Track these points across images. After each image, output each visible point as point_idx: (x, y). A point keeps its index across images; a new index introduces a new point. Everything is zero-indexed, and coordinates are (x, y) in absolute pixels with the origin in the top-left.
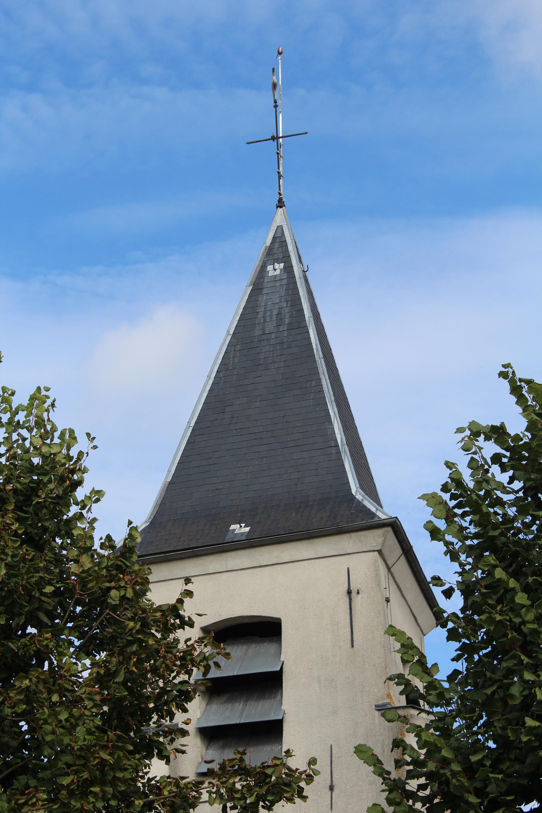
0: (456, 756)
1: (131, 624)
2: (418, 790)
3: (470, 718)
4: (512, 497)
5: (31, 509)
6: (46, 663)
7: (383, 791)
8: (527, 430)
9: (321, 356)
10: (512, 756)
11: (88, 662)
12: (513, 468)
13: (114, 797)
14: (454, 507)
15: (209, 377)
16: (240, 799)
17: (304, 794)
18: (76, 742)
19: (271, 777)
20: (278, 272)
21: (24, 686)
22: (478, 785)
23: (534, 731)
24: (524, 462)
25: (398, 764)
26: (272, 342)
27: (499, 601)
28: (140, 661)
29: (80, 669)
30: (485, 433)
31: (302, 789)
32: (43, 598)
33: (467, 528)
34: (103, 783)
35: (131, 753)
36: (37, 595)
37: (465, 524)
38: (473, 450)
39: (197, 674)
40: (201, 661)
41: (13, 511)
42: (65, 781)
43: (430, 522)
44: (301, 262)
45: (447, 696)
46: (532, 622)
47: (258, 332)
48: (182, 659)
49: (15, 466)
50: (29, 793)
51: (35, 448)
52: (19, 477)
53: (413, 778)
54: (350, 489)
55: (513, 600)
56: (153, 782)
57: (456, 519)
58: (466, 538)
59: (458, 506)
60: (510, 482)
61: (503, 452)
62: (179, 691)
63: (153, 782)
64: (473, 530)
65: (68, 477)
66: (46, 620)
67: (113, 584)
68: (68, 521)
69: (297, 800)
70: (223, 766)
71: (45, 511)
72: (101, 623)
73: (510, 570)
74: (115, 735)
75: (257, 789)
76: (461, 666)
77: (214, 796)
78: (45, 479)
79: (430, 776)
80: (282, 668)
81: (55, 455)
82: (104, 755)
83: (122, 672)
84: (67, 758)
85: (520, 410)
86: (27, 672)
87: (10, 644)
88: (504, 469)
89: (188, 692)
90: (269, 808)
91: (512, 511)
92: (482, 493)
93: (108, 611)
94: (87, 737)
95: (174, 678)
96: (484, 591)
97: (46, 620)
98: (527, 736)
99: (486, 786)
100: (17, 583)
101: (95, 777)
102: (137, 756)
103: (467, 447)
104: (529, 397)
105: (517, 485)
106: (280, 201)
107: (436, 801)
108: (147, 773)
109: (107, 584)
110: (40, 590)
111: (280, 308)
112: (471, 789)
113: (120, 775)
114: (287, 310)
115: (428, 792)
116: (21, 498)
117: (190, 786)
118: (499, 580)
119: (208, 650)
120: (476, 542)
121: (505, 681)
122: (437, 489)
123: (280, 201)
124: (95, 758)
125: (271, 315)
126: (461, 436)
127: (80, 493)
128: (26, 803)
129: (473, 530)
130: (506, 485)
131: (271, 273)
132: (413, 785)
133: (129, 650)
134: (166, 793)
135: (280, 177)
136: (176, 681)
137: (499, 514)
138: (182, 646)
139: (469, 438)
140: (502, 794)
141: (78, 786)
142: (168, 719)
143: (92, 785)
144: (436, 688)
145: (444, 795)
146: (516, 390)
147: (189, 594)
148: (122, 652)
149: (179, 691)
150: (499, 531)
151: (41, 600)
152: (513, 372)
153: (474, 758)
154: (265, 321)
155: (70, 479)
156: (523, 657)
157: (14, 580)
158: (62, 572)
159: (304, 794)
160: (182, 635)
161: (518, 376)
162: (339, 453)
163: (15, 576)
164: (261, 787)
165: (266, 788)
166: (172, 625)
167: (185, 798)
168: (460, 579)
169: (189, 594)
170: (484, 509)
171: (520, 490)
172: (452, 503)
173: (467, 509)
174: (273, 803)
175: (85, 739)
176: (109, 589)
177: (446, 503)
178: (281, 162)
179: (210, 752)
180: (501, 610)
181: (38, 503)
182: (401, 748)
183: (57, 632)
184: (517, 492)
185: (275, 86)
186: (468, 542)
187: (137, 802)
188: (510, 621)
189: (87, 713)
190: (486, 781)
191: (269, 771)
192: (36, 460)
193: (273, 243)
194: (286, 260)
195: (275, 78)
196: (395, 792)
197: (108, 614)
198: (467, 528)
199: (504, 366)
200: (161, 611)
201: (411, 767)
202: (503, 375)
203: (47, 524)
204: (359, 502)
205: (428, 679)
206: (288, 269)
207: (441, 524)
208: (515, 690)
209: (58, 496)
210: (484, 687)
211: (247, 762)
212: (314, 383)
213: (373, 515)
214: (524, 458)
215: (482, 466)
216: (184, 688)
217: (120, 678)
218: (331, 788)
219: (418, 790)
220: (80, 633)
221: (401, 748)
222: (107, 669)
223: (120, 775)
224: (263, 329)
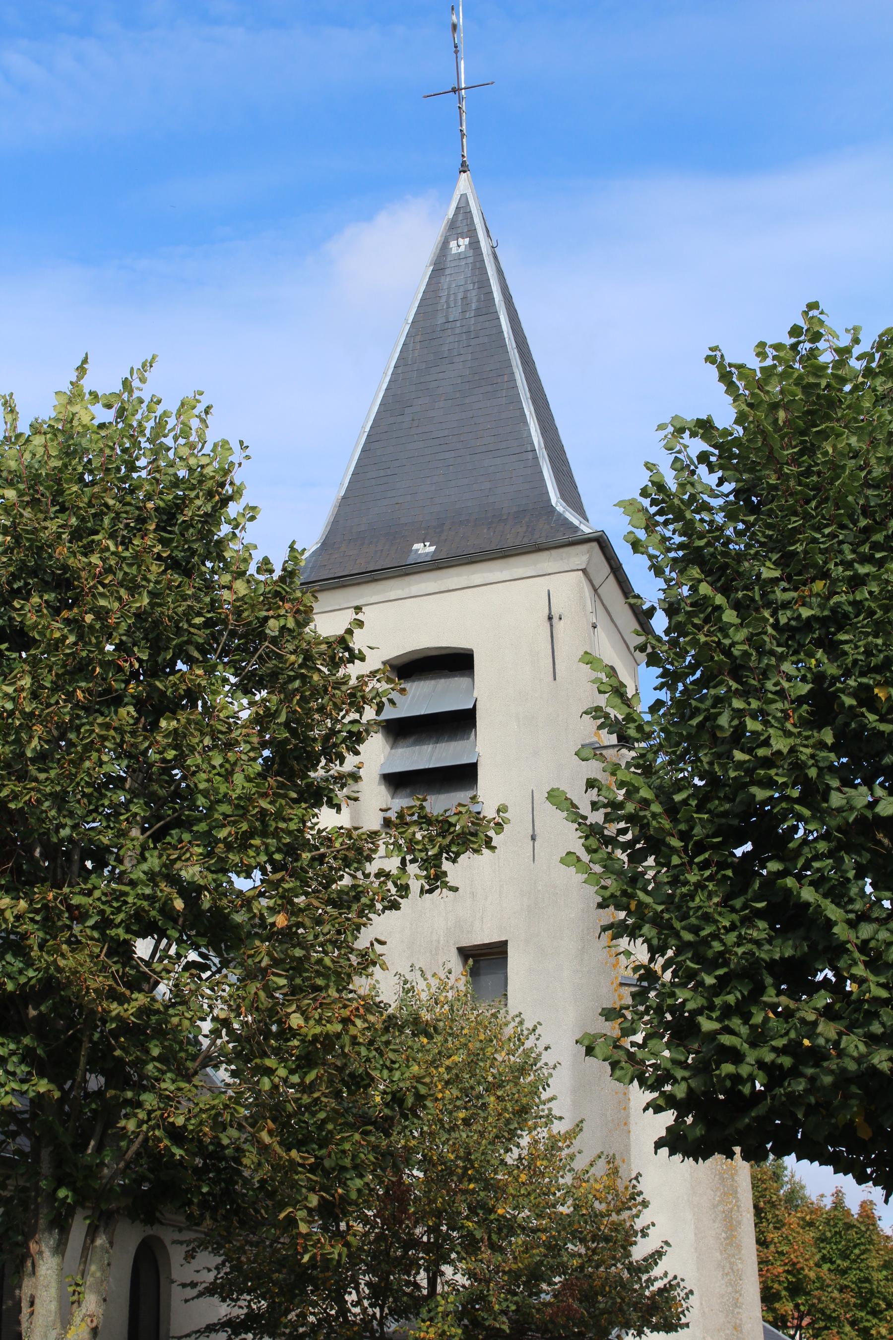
0: (657, 796)
1: (293, 658)
2: (618, 835)
3: (674, 753)
4: (720, 502)
5: (176, 529)
6: (200, 703)
7: (580, 837)
8: (737, 422)
9: (514, 345)
10: (722, 795)
11: (245, 702)
12: (722, 467)
13: (279, 850)
14: (655, 515)
15: (385, 373)
16: (420, 851)
17: (493, 844)
18: (234, 790)
19: (455, 825)
20: (462, 249)
21: (171, 728)
22: (683, 827)
23: (745, 766)
24: (735, 461)
25: (595, 806)
26: (457, 331)
27: (707, 620)
28: (304, 700)
29: (237, 709)
30: (690, 429)
31: (491, 839)
32: (192, 630)
33: (671, 538)
34: (264, 834)
35: (296, 801)
36: (186, 626)
37: (668, 534)
38: (677, 448)
39: (369, 713)
40: (374, 698)
41: (155, 531)
42: (222, 834)
43: (631, 532)
44: (489, 236)
45: (647, 729)
46: (743, 643)
47: (440, 320)
48: (353, 695)
49: (157, 480)
50: (182, 848)
51: (181, 458)
52: (161, 493)
53: (612, 821)
54: (549, 500)
55: (720, 619)
56: (324, 834)
57: (658, 528)
58: (669, 550)
59: (660, 512)
60: (720, 484)
61: (712, 450)
62: (349, 732)
63: (324, 834)
64: (678, 539)
65: (217, 491)
66: (196, 654)
67: (271, 613)
68: (219, 542)
69: (485, 851)
70: (401, 815)
71: (191, 530)
72: (260, 657)
73: (719, 585)
74: (276, 781)
75: (440, 839)
76: (664, 695)
77: (392, 847)
78: (193, 494)
79: (631, 819)
80: (475, 706)
81: (203, 467)
82: (264, 804)
83: (284, 710)
84: (225, 808)
85: (730, 399)
86: (174, 712)
87: (158, 683)
88: (711, 470)
89: (360, 733)
90: (454, 861)
91: (720, 518)
92: (686, 497)
93: (267, 644)
94: (246, 785)
95: (344, 717)
96: (689, 609)
97: (196, 654)
98: (735, 770)
99: (692, 828)
100: (162, 613)
101: (255, 828)
102: (304, 805)
103: (669, 446)
104: (741, 384)
105: (727, 487)
106: (463, 164)
107: (638, 846)
108: (317, 824)
109: (264, 613)
110: (188, 621)
111: (466, 291)
112: (674, 832)
113: (283, 825)
114: (474, 293)
115: (629, 836)
116: (165, 517)
117: (364, 837)
118: (705, 597)
119: (383, 686)
120: (681, 553)
121: (712, 711)
122: (636, 495)
123: (463, 164)
124: (254, 807)
125: (455, 300)
126: (662, 434)
127: (233, 510)
128: (179, 858)
129: (678, 539)
130: (714, 487)
131: (454, 251)
132: (611, 830)
133: (290, 687)
134: (337, 845)
135: (463, 135)
136: (346, 721)
137: (705, 521)
138: (353, 682)
139: (673, 434)
140: (708, 836)
141: (236, 838)
142: (337, 762)
143: (252, 838)
144: (634, 721)
145: (648, 839)
146: (725, 377)
147: (360, 624)
148: (282, 690)
149: (349, 732)
150: (705, 540)
151: (190, 633)
152: (722, 356)
153: (678, 798)
154: (448, 307)
155: (220, 494)
156: (731, 683)
157: (159, 609)
158: (213, 601)
159: (493, 844)
160: (354, 670)
161: (728, 360)
162: (536, 458)
163: (160, 605)
164: (444, 837)
165: (449, 838)
166: (341, 658)
167: (359, 851)
168: (662, 596)
169: (360, 624)
170: (688, 515)
171: (730, 493)
172: (653, 510)
173: (671, 516)
174: (458, 855)
175: (243, 788)
176: (266, 619)
177: (647, 510)
178: (464, 118)
179: (397, 801)
180: (708, 631)
181: (184, 521)
182: (596, 790)
183: (210, 670)
184: (727, 495)
185: (454, 27)
186: (672, 554)
187: (304, 855)
188: (719, 643)
189: (244, 757)
190: (691, 822)
191: (453, 820)
192: (182, 473)
193: (456, 214)
194: (472, 233)
195: (454, 18)
196: (591, 838)
197: (268, 647)
198: (671, 538)
199: (711, 349)
200: (327, 643)
201: (609, 810)
202: (710, 359)
203: (195, 546)
204: (560, 515)
205: (627, 710)
206: (475, 245)
207: (641, 534)
208: (723, 720)
209: (206, 514)
210: (692, 717)
211: (428, 810)
212: (506, 378)
213: (576, 529)
214: (735, 456)
215: (688, 466)
216: (355, 729)
217: (282, 719)
218: (533, 838)
219: (618, 835)
220: (236, 669)
221: (596, 790)
222: (267, 709)
223: (283, 825)
224: (447, 316)
